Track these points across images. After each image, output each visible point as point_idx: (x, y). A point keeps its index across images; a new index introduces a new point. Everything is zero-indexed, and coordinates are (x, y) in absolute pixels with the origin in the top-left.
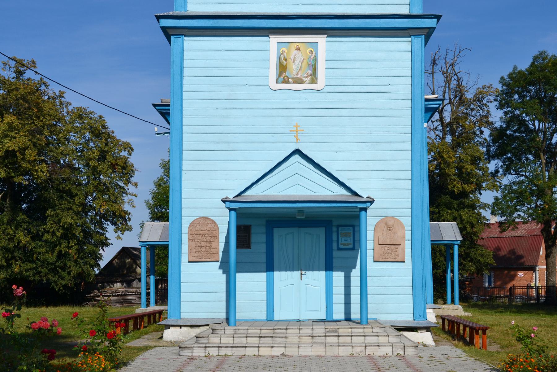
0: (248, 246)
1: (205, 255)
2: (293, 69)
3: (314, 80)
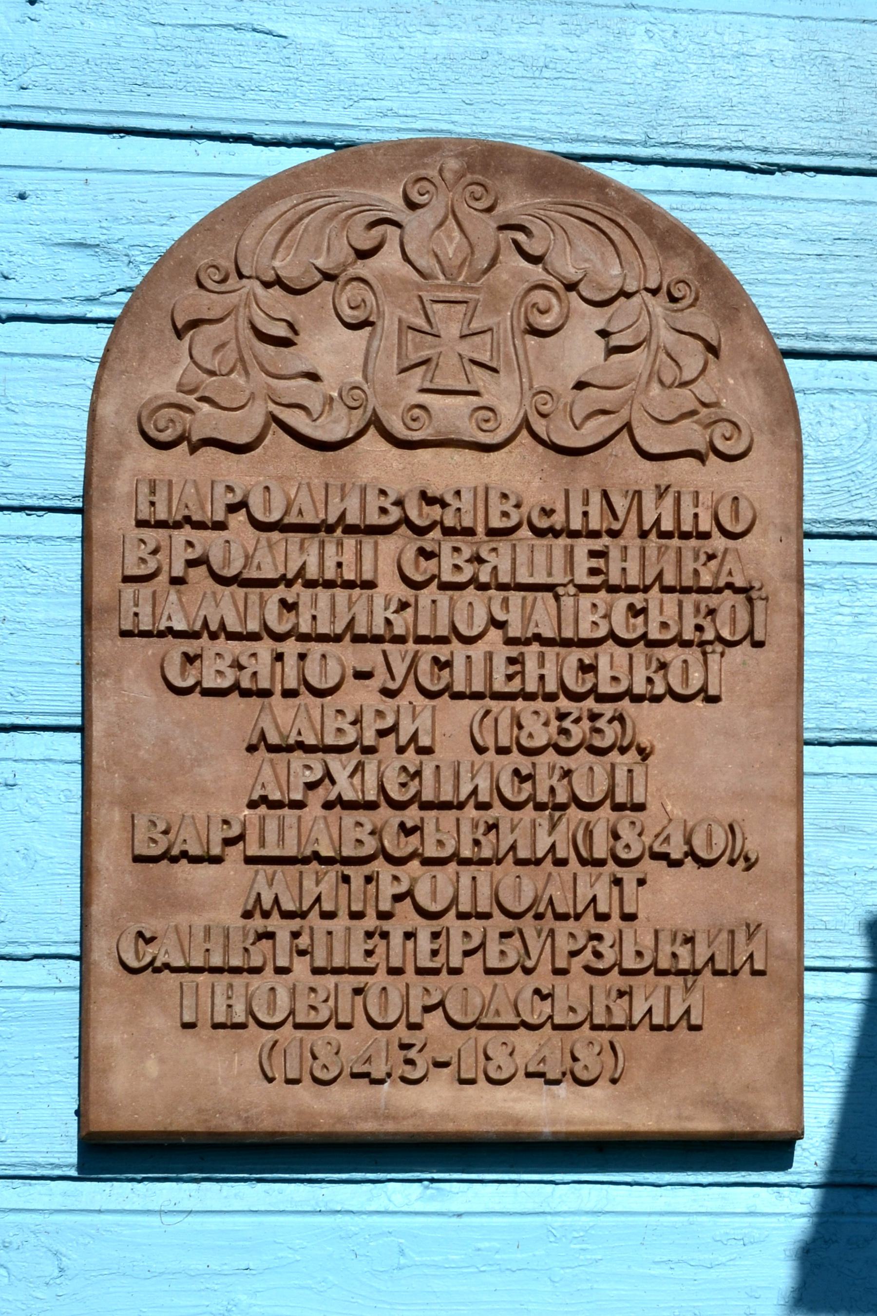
1: (472, 992)
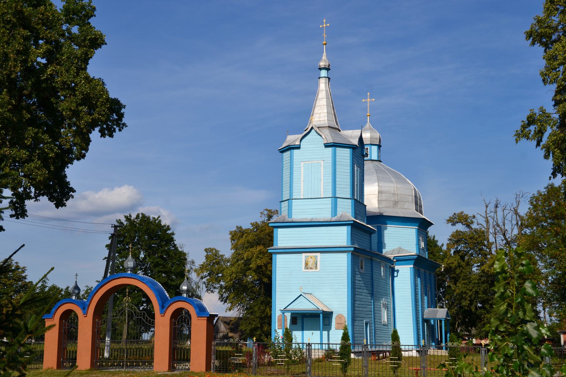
0: (296, 324)
2: (310, 265)
3: (316, 268)
